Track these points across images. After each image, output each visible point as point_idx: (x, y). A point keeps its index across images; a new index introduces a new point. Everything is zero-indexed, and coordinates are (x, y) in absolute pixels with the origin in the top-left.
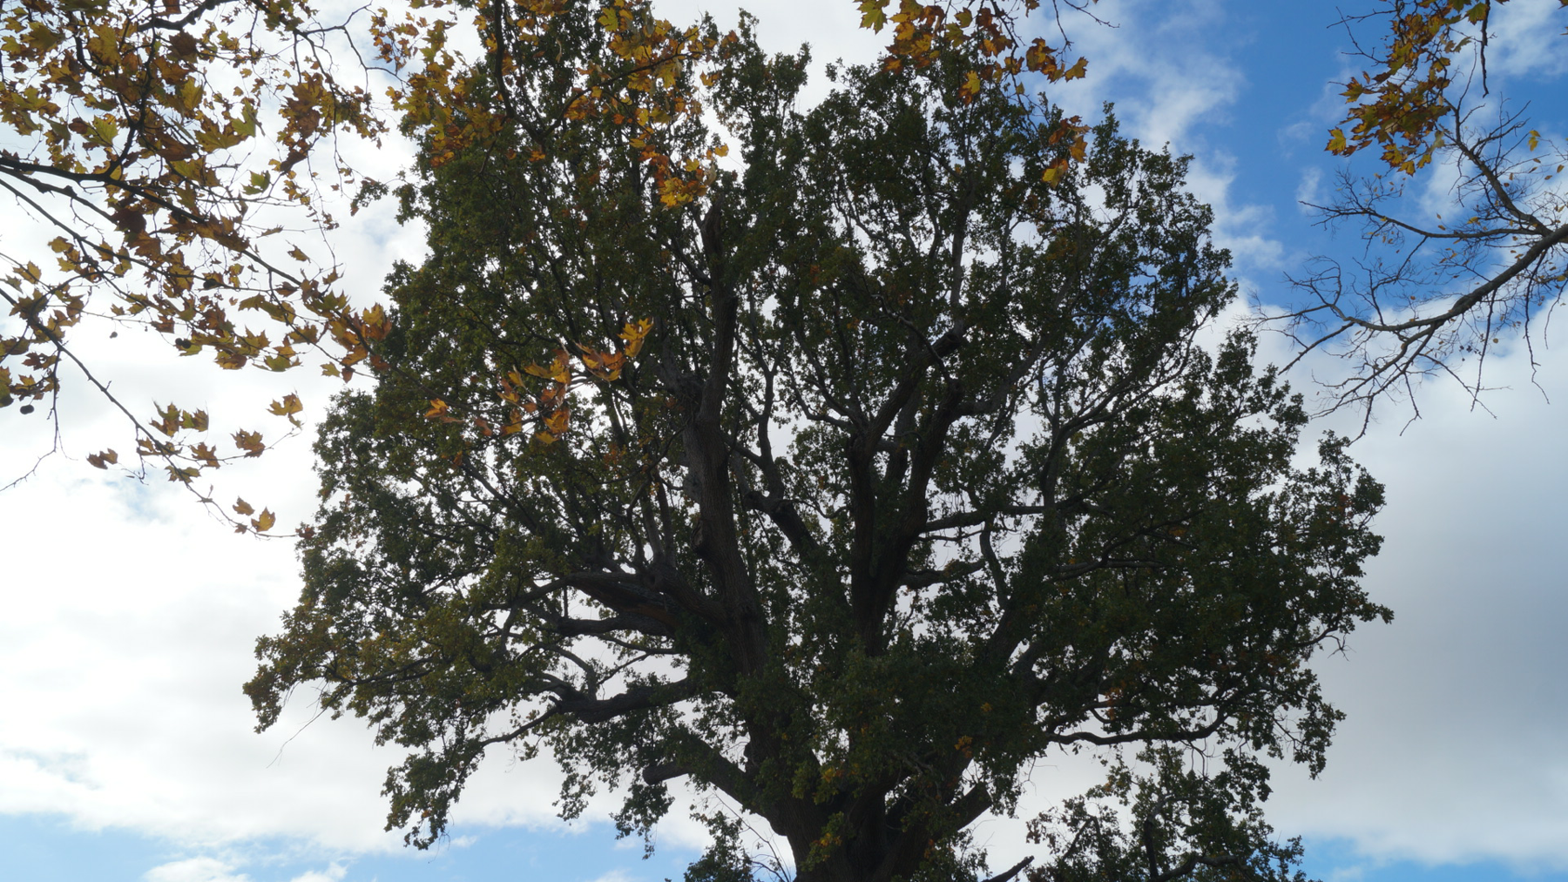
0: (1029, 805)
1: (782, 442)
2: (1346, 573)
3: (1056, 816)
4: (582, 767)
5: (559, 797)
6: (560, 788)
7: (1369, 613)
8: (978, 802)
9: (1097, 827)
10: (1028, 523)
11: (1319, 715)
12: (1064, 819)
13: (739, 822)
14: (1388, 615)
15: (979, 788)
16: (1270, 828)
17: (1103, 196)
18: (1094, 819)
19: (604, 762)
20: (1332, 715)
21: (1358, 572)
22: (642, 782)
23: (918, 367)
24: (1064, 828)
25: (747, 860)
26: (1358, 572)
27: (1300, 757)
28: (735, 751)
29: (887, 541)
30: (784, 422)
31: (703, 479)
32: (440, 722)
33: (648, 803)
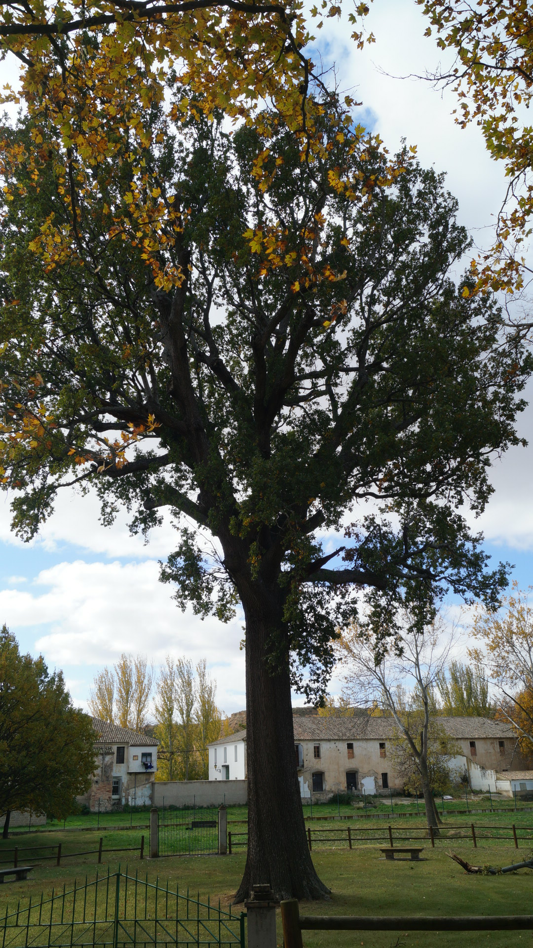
0: (346, 519)
1: (218, 316)
2: (507, 419)
3: (360, 524)
4: (110, 497)
5: (100, 516)
6: (100, 511)
7: (515, 441)
8: (317, 520)
9: (380, 529)
10: (353, 375)
11: (485, 488)
12: (364, 526)
13: (195, 532)
14: (525, 443)
15: (319, 512)
16: (469, 528)
17: (357, 326)
18: (378, 525)
19: (123, 495)
20: (491, 490)
21: (513, 420)
22: (142, 508)
23: (298, 292)
24: (364, 530)
25: (199, 551)
26: (513, 420)
27: (473, 507)
28: (193, 496)
29: (276, 383)
30: (220, 305)
31: (173, 354)
32: (31, 476)
33: (148, 519)
